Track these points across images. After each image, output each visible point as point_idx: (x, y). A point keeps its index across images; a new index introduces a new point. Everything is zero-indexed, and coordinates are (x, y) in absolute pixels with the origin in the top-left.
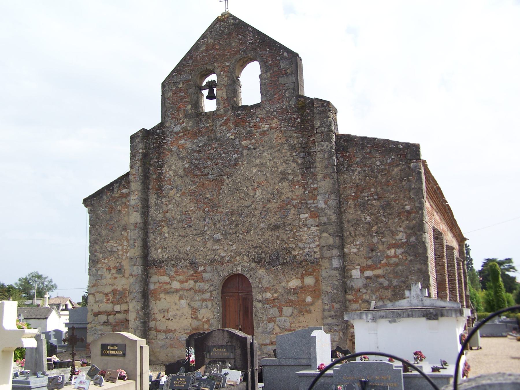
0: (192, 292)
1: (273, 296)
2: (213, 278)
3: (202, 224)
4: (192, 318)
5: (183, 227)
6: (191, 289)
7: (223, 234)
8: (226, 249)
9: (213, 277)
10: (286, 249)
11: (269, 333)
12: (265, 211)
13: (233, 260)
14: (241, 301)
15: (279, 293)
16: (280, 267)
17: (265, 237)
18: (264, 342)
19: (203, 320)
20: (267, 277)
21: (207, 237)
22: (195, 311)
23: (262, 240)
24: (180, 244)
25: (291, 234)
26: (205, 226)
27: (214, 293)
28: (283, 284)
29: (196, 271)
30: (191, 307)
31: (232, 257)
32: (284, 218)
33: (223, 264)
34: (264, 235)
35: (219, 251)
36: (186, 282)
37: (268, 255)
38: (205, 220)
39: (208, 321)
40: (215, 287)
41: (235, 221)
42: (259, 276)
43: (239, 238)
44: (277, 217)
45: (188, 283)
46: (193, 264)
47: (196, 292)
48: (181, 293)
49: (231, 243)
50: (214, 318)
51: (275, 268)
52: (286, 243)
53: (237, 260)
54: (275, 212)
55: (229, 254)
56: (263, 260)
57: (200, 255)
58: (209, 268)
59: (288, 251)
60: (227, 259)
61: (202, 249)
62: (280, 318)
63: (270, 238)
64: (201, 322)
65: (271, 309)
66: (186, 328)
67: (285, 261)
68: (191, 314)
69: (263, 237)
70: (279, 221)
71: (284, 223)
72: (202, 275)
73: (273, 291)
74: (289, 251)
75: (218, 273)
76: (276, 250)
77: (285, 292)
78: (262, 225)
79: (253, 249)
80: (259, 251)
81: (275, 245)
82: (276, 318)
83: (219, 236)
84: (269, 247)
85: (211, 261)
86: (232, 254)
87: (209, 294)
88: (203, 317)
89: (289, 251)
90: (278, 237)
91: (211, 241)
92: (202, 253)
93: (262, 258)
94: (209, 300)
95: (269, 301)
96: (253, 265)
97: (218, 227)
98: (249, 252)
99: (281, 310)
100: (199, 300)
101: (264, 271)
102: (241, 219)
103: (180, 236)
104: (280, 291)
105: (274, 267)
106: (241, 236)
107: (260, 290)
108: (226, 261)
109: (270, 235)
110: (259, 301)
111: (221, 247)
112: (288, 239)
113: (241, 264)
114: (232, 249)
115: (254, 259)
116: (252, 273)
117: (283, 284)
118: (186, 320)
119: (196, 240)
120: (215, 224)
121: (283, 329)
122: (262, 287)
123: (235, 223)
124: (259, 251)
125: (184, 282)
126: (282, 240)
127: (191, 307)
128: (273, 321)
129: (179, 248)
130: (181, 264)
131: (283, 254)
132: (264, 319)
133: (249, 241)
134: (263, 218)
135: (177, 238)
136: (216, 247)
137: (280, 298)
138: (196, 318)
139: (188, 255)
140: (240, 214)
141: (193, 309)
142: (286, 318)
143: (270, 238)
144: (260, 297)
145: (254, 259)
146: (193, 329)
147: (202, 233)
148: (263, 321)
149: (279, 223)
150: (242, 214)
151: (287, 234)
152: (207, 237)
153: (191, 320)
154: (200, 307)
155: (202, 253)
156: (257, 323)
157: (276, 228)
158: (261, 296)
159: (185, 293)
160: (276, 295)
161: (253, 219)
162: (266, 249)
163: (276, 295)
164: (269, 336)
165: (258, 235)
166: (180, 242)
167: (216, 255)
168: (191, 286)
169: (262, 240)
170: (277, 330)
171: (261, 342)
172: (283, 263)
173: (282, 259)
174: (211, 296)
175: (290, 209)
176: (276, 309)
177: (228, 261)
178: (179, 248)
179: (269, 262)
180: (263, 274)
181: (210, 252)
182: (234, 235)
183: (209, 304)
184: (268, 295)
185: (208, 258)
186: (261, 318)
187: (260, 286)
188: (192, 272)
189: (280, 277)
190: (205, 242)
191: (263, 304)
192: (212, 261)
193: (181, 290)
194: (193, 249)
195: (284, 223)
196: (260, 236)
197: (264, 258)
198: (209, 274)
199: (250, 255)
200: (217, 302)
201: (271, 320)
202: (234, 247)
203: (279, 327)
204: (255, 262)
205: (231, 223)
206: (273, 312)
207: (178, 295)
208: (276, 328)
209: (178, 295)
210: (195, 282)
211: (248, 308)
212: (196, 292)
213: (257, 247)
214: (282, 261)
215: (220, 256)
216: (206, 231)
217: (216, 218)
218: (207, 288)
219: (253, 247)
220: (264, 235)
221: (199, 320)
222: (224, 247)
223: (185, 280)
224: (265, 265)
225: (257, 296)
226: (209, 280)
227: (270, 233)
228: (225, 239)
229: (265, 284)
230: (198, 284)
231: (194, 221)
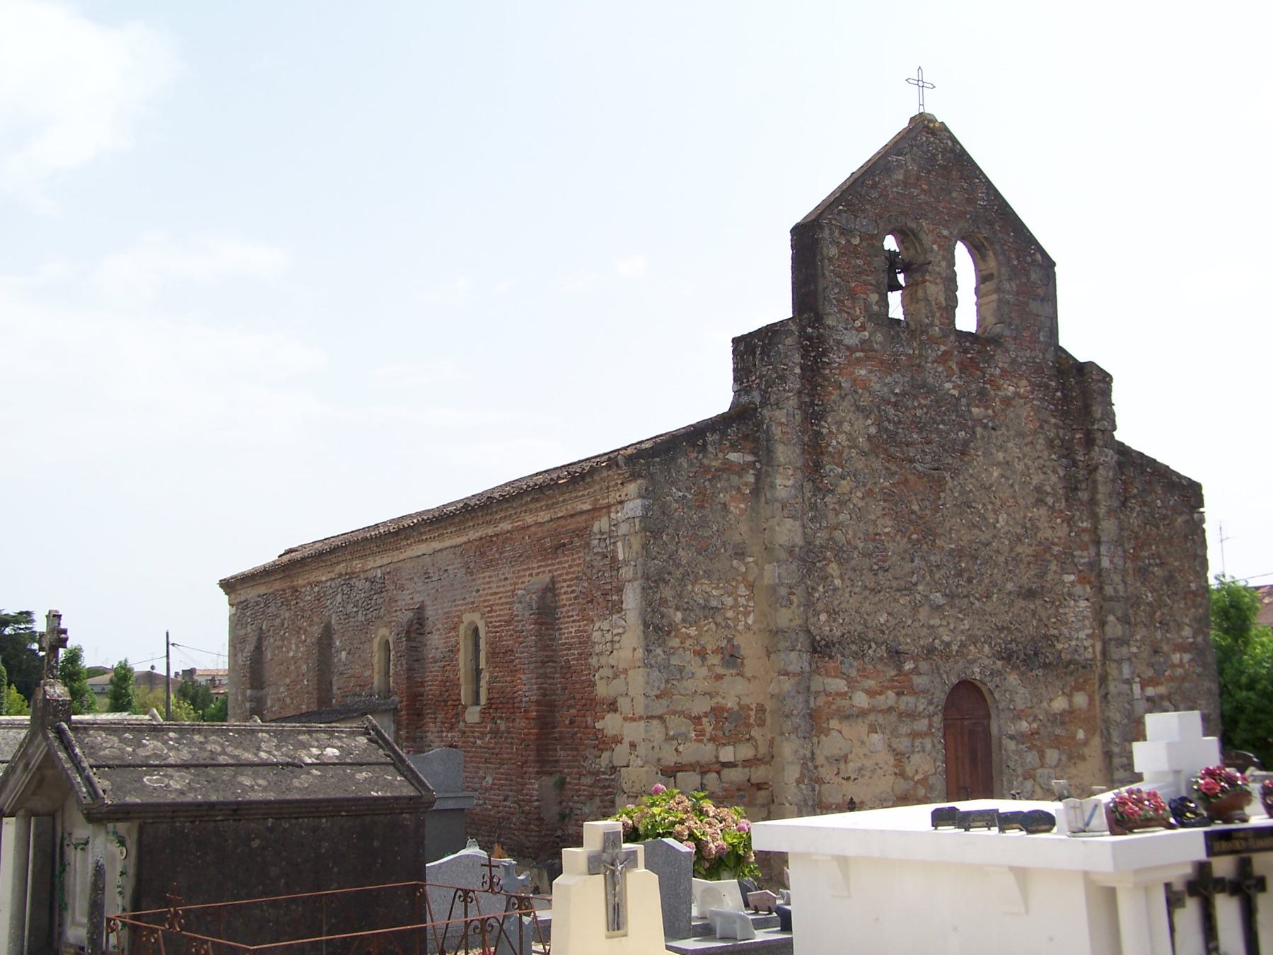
0: (893, 717)
3: (908, 567)
6: (891, 709)
8: (952, 626)
10: (1046, 637)
12: (1014, 559)
16: (1040, 672)
17: (1015, 610)
19: (916, 778)
20: (1021, 690)
24: (867, 607)
28: (1045, 704)
39: (925, 779)
45: (883, 697)
46: (896, 655)
51: (1034, 673)
54: (1029, 563)
58: (924, 666)
61: (909, 622)
66: (884, 796)
72: (910, 680)
76: (1033, 638)
83: (938, 598)
87: (926, 721)
90: (1034, 613)
94: (926, 734)
97: (937, 576)
99: (1042, 756)
110: (1012, 737)
111: (944, 623)
123: (966, 575)
134: (1010, 571)
137: (1042, 731)
144: (1012, 730)
147: (909, 589)
151: (1047, 609)
153: (893, 777)
163: (1035, 725)
168: (891, 703)
174: (931, 726)
181: (925, 632)
184: (1024, 726)
188: (894, 673)
190: (915, 608)
192: (930, 651)
194: (893, 622)
198: (925, 677)
204: (1003, 658)
205: (959, 574)
213: (1003, 628)
215: (942, 641)
216: (915, 584)
218: (921, 708)
230: (904, 698)
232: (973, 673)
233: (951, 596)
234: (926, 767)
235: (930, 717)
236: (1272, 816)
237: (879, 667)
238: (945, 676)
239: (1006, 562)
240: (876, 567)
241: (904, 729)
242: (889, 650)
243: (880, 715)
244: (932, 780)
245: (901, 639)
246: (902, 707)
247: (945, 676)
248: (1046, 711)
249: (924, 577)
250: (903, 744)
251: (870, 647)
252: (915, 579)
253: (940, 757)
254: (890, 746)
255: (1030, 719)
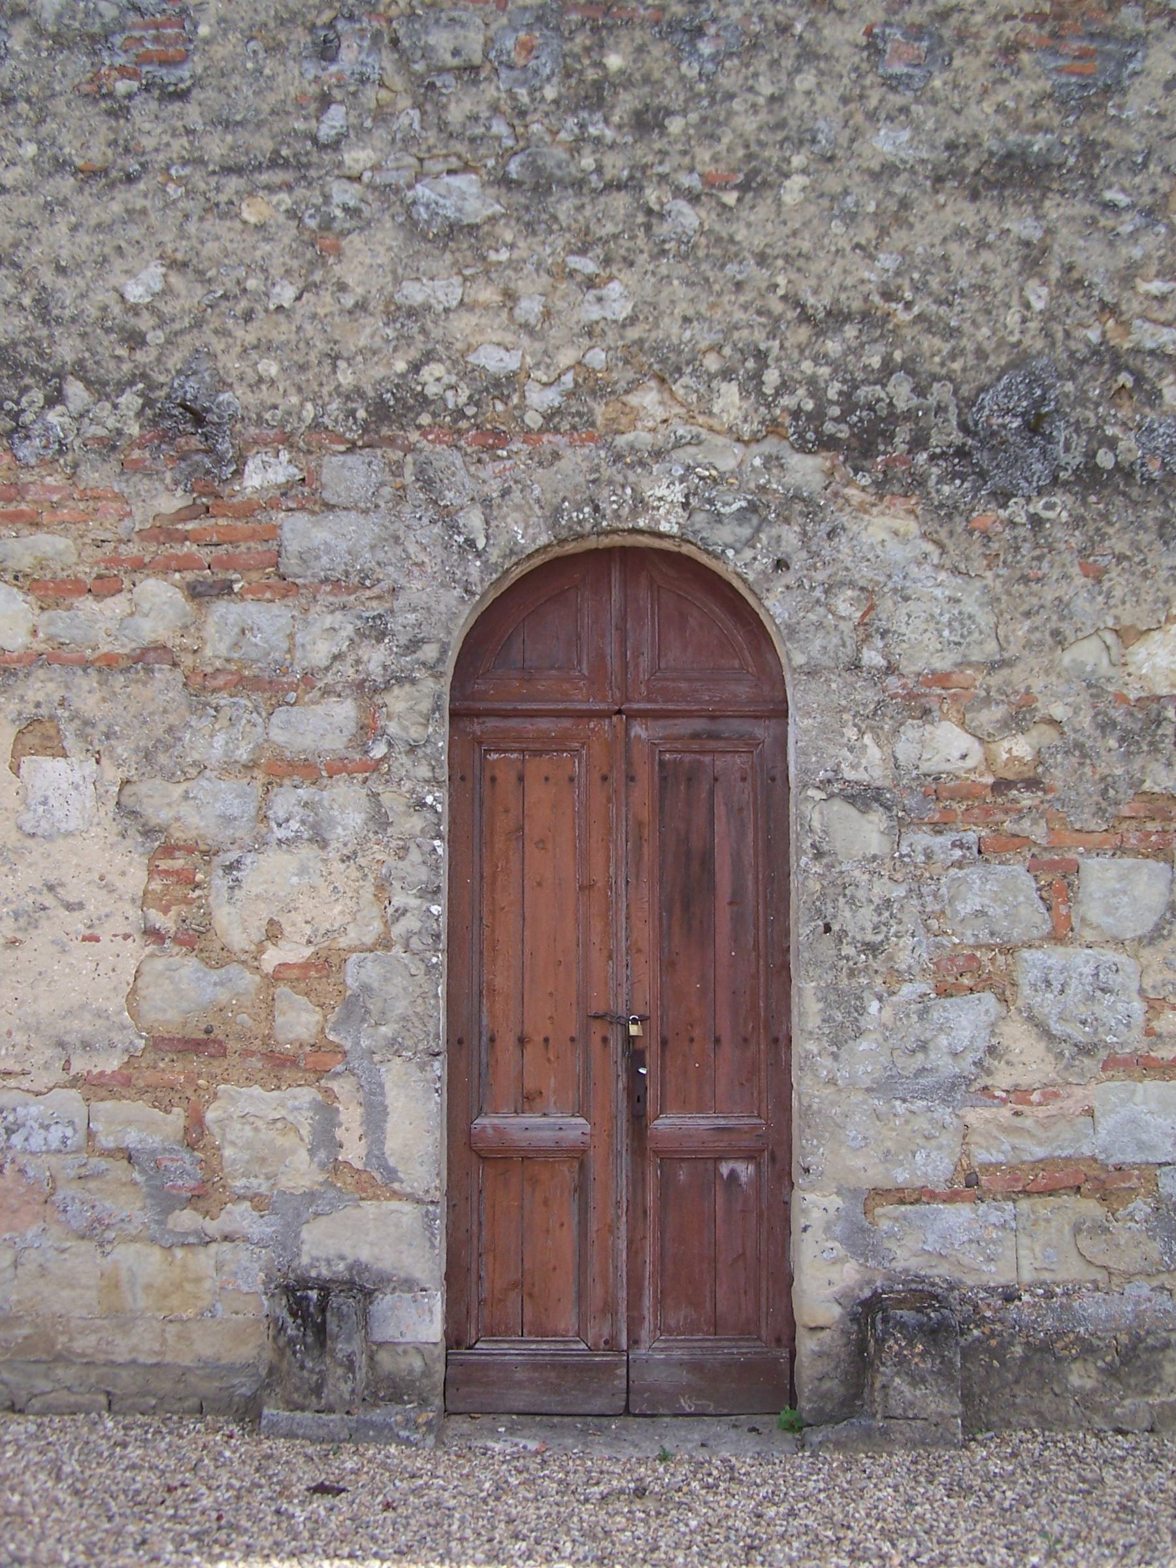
0: (163, 689)
1: (989, 761)
2: (408, 563)
3: (296, 77)
4: (153, 934)
5: (97, 93)
6: (147, 658)
7: (506, 182)
8: (530, 308)
9: (391, 553)
10: (1108, 357)
11: (951, 1090)
12: (916, 32)
13: (600, 411)
14: (643, 794)
15: (1048, 735)
16: (1059, 508)
17: (921, 239)
18: (901, 1176)
19: (272, 958)
20: (934, 587)
21: (343, 194)
22: (181, 865)
23: (887, 260)
24: (57, 237)
25: (1149, 241)
26: (325, 101)
27: (398, 700)
28: (1088, 654)
29: (209, 491)
30: (148, 832)
31: (591, 385)
32: (1087, 107)
33: (500, 438)
34: (901, 221)
35: (462, 324)
36: (104, 586)
37: (940, 392)
38: (326, 51)
39: (325, 964)
40: (414, 645)
41: (625, 81)
42: (864, 573)
43: (663, 229)
44: (1031, 87)
45: (117, 605)
46: (190, 427)
47: (200, 687)
48: (40, 689)
49: (586, 265)
50: (385, 943)
51: (1017, 509)
52: (1108, 309)
53: (635, 416)
54: (1010, 51)
55: (567, 357)
56: (903, 434)
57: (265, 347)
58: (349, 474)
59: (1125, 379)
60: (541, 399)
61: (286, 293)
62: (1053, 957)
63: (958, 251)
64: (248, 980)
65: (973, 874)
66: (83, 1026)
67: (1105, 459)
68: (145, 899)
69: (900, 237)
70: (1037, 128)
71: (1090, 149)
72: (272, 533)
73: (997, 712)
74: (1139, 378)
75: (448, 518)
76: (1021, 360)
77: (1106, 726)
78: (886, 142)
79: (804, 333)
80: (856, 351)
81: (1012, 319)
82: (1009, 950)
83: (466, 196)
84: (953, 333)
85: (381, 412)
86: (597, 358)
87: (345, 711)
88: (273, 932)
89: (1139, 378)
90: (1033, 259)
91: (387, 236)
92: (283, 332)
93: (893, 417)
94: (338, 768)
95: (959, 795)
96: (806, 470)
97: (455, 114)
98: (761, 356)
99: (1059, 884)
100: (228, 768)
101: (912, 527)
102: (690, 69)
103: (61, 165)
104: (1059, 711)
105: (1002, 497)
106: (688, 217)
107: (871, 696)
108: (533, 420)
109: (961, 234)
110: (864, 797)
111: (488, 294)
112: (1128, 276)
113: (687, 455)
114: (594, 313)
115: (818, 416)
116: (790, 536)
117: (1088, 654)
118: (81, 951)
119: (229, 212)
120: (426, 92)
121: (1085, 1050)
122: (891, 669)
123: (626, 103)
124: (856, 351)
125: (81, 588)
126: (1073, 282)
127: (148, 832)
128: (986, 983)
129: (47, 276)
130: (53, 417)
131: (1082, 399)
132: (904, 960)
133: (762, 259)
134: (892, 83)
135: (31, 188)
136: (437, 288)
137: (1058, 775)
138: (195, 938)
139: (135, 340)
140: (675, 26)
141: (169, 850)
142: (1110, 955)
143: (958, 251)
144: (869, 763)
145: (818, 416)
146: (158, 1043)
147: (299, 162)
148: (897, 976)
149: (1039, 143)
150: (698, 32)
151: (1112, 239)
152: (343, 194)
153: (135, 950)
154: (243, 831)
155: (283, 332)
156: (833, 996)
157: (1017, 174)
158: (874, 753)
159: (88, 696)
160: (1019, 748)
161: (806, 80)
162: (930, 343)
163: (1019, 748)
164: (943, 1113)
165: (850, 218)
166: (63, 223)
167: (429, 357)
168: (151, 629)
169: (887, 260)
170: (1029, 1061)
171: (869, 1170)
172: (1089, 478)
173: (1080, 443)
174: (367, 730)
175: (1139, 40)
176: (1019, 869)
177: (551, 416)
178: (47, 276)
179: (962, 453)
180: (897, 552)
181: (370, 330)
182: (621, 202)
183: (346, 807)
184: (949, 746)
185: (346, 377)
186: (872, 949)
187: (872, 657)
188: (171, 502)
189: (1064, 591)
190: (321, 242)
191: (900, 826)
192: (387, 415)
193: (37, 660)
194: (189, 295)
195: (1090, 149)
196: (867, 233)
197: (909, 415)
198: (350, 523)
199: (772, 377)
200: (419, 787)
201: (964, 973)
202: (617, 301)
203: (1047, 1034)
204: (828, 443)
205: (595, 97)
206: (993, 896)
207: (229, 138)
208: (1018, 1037)
209: (13, 707)
210: (196, 593)
211: (707, 859)
212: (200, 687)
213: (837, 317)
214: (1076, 459)
215: (469, 373)
216: (335, 145)
217: (441, 40)
218: (320, 652)
219: (805, 317)
220: (901, 221)
221: (223, 958)
222: (510, 296)
223: (86, 572)
224: (920, 481)
225: (823, 737)
226: (344, 584)
227: (969, 215)
228: (530, 228)
229: (923, 648)
230: (224, 611)
231: (219, 51)
232: (640, 504)
233: (532, 189)
234: (335, 913)
235: (366, 690)
236: (910, 2)
237: (96, 476)
238: (473, 520)
239: (873, 46)
240: (122, 87)
241: (213, 743)
242: (154, 413)
243: (91, 681)
244: (359, 972)
245: (232, 364)
246: (217, 646)
247: (473, 520)
248: (1094, 688)
249: (382, 115)
250: (204, 807)
251: (56, 399)
252: (335, 119)
253: (415, 868)
254: (126, 811)
255: (990, 716)
